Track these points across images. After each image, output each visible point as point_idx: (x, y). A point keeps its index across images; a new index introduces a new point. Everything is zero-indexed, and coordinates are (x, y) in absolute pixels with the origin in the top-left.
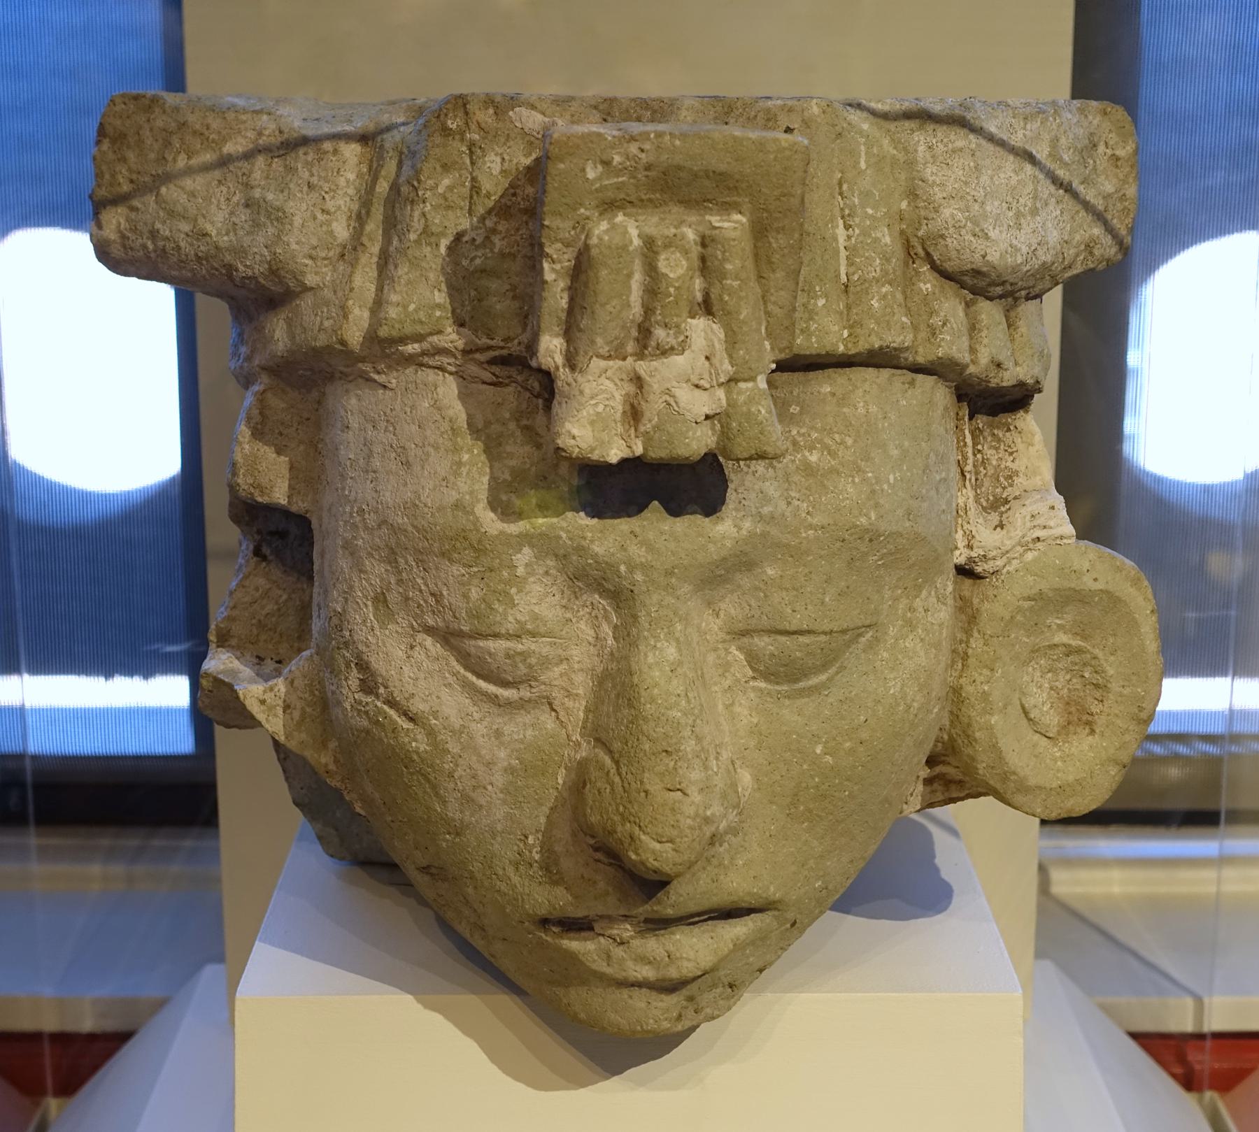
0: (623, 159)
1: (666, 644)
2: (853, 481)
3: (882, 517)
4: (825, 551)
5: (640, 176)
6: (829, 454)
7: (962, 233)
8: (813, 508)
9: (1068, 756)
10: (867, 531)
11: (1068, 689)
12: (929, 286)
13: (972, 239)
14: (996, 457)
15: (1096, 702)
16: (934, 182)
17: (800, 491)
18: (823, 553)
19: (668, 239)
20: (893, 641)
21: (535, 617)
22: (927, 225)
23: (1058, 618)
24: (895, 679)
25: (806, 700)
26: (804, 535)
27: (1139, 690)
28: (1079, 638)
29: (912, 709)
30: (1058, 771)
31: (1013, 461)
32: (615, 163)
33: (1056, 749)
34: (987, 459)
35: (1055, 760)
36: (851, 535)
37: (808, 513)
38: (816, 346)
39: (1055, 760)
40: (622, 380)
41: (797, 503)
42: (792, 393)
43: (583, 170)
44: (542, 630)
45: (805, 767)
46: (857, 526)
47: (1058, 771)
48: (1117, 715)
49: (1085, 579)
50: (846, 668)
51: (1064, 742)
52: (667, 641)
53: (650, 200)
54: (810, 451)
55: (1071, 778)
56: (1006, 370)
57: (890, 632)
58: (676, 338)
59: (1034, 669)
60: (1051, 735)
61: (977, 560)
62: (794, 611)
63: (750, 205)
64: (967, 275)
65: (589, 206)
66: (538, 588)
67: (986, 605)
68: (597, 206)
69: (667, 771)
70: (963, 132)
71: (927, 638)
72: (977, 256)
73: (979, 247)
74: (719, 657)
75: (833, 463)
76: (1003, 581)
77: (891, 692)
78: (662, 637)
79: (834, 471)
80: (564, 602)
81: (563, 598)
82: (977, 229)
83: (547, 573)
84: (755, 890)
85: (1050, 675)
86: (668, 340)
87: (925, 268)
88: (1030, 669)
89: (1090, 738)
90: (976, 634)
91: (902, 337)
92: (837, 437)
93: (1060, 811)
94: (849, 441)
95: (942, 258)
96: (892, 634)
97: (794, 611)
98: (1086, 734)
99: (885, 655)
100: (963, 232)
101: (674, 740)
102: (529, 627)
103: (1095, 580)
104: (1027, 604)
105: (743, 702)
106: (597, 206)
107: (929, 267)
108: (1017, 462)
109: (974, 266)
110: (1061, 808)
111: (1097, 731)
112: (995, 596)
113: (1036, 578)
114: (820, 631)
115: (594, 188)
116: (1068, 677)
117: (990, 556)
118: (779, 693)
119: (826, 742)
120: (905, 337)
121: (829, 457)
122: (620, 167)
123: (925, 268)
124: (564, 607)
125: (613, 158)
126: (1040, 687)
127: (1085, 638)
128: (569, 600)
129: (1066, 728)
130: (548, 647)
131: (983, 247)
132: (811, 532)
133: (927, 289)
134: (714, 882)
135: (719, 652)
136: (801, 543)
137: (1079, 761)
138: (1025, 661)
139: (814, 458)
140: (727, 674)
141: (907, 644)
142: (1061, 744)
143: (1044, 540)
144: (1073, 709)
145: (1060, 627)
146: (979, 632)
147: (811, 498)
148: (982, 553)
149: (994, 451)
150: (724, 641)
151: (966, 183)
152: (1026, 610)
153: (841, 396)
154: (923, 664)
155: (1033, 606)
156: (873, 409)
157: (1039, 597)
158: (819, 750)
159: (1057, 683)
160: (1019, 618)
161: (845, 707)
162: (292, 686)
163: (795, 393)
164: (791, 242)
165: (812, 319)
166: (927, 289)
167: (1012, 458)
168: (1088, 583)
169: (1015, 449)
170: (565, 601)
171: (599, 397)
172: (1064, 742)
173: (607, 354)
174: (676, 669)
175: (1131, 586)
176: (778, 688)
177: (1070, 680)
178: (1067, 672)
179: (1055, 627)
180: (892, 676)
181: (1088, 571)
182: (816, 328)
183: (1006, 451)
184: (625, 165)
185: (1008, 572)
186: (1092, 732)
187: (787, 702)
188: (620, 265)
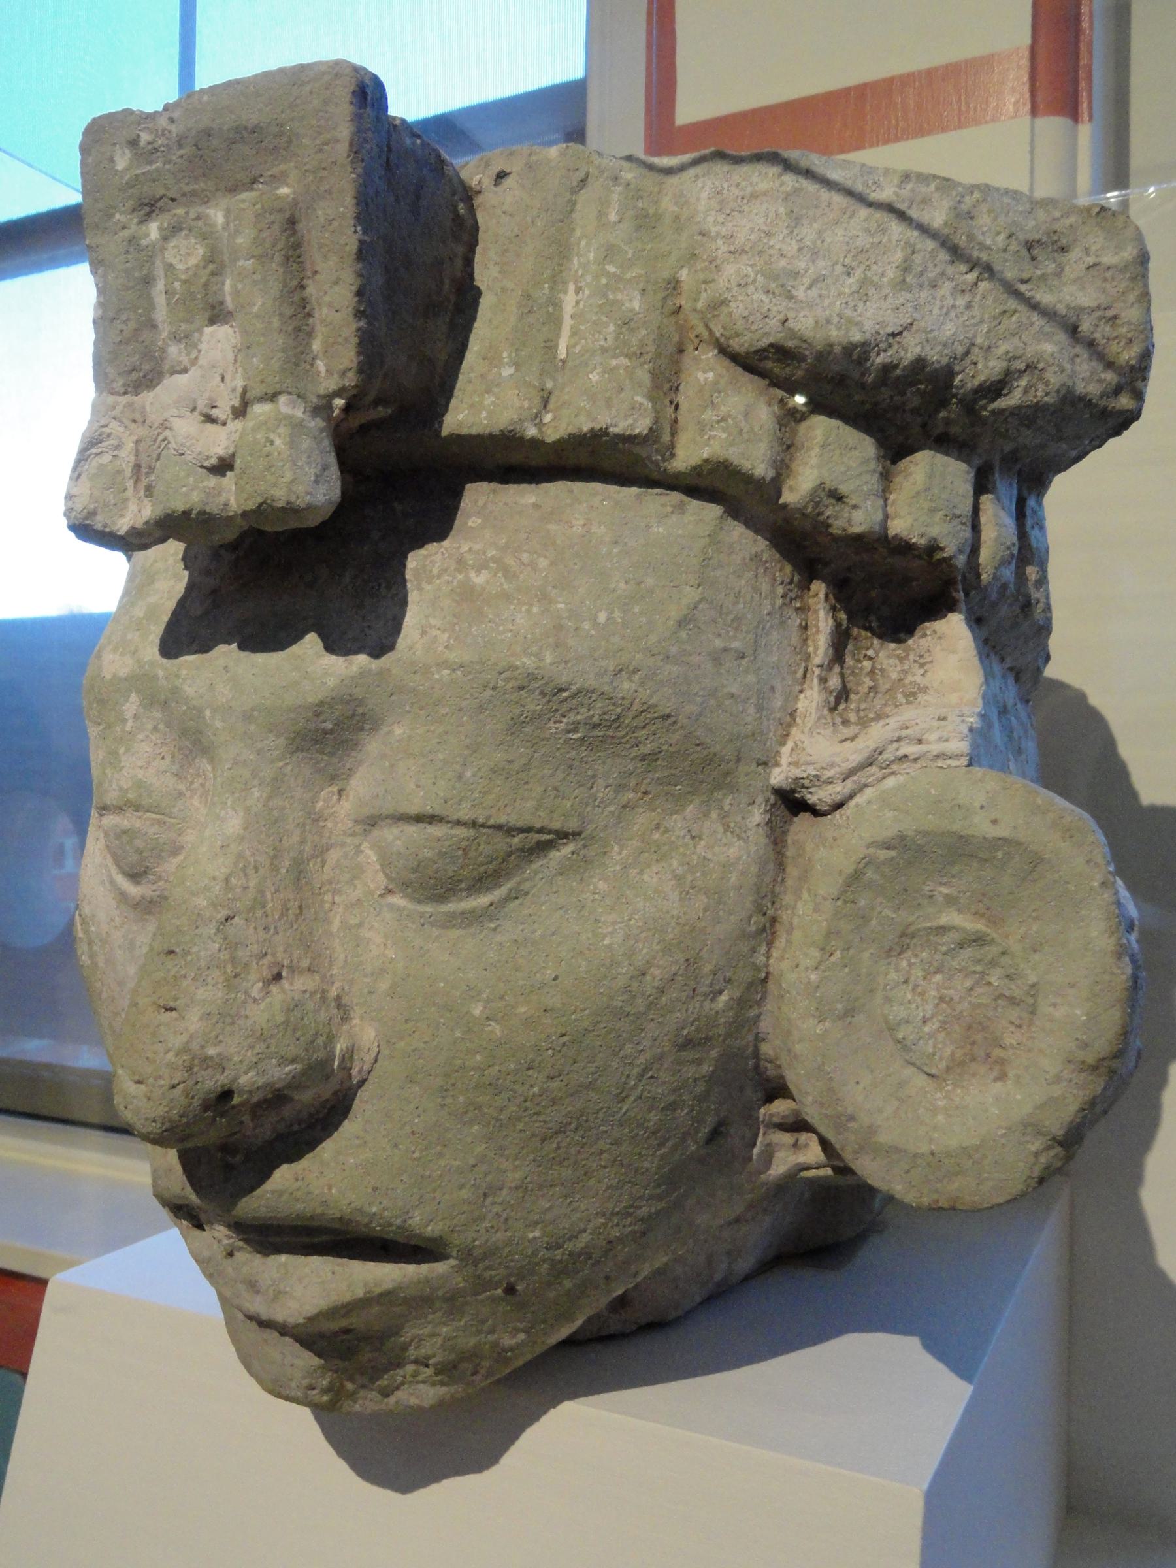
0: (153, 136)
1: (231, 812)
2: (528, 611)
3: (566, 662)
4: (468, 702)
5: (174, 158)
6: (505, 576)
7: (749, 292)
8: (455, 639)
9: (957, 1108)
10: (532, 677)
11: (970, 1002)
12: (711, 375)
13: (764, 297)
14: (899, 668)
15: (1012, 1028)
16: (718, 234)
17: (445, 618)
18: (464, 703)
19: (176, 218)
20: (618, 868)
21: (139, 784)
22: (706, 290)
23: (941, 884)
24: (614, 923)
25: (461, 932)
26: (437, 676)
27: (1078, 1012)
28: (983, 921)
29: (648, 978)
30: (935, 1128)
31: (923, 675)
32: (142, 143)
33: (939, 1095)
34: (882, 670)
35: (934, 1111)
36: (507, 680)
37: (446, 647)
38: (486, 422)
39: (934, 1111)
40: (134, 421)
41: (434, 632)
42: (476, 502)
43: (112, 160)
44: (146, 802)
45: (458, 1034)
46: (517, 668)
47: (935, 1128)
48: (1041, 1051)
49: (977, 819)
50: (527, 893)
51: (955, 1085)
52: (233, 809)
53: (193, 193)
54: (478, 572)
55: (953, 1143)
56: (855, 507)
57: (614, 854)
58: (188, 354)
59: (910, 965)
60: (933, 1071)
61: (806, 783)
62: (418, 786)
63: (297, 171)
64: (767, 358)
65: (123, 209)
66: (146, 747)
67: (822, 852)
68: (134, 210)
69: (165, 979)
70: (773, 170)
71: (689, 878)
72: (774, 323)
73: (775, 309)
74: (345, 855)
75: (505, 587)
76: (848, 817)
77: (606, 942)
78: (229, 803)
79: (506, 597)
80: (175, 768)
81: (173, 762)
82: (773, 285)
83: (155, 728)
84: (374, 1210)
85: (938, 978)
86: (181, 359)
87: (710, 355)
88: (904, 963)
89: (999, 1084)
90: (805, 895)
91: (630, 421)
92: (525, 557)
93: (935, 1196)
94: (543, 563)
95: (727, 334)
96: (618, 858)
97: (418, 786)
98: (992, 1077)
99: (602, 885)
100: (751, 289)
101: (188, 938)
102: (131, 796)
103: (994, 822)
104: (883, 854)
105: (376, 924)
106: (134, 210)
107: (716, 352)
108: (929, 675)
109: (771, 340)
110: (937, 1191)
111: (1011, 1075)
112: (835, 840)
113: (896, 813)
114: (455, 818)
115: (124, 182)
116: (968, 983)
117: (825, 777)
118: (422, 915)
119: (488, 1001)
120: (636, 421)
121: (503, 580)
122: (150, 147)
123: (710, 355)
124: (176, 775)
125: (138, 136)
126: (922, 994)
127: (994, 922)
128: (182, 767)
129: (958, 1067)
130: (157, 826)
131: (781, 308)
132: (446, 672)
133: (706, 379)
134: (297, 1180)
135: (347, 849)
136: (433, 688)
137: (974, 1118)
138: (891, 949)
139: (479, 579)
140: (356, 882)
141: (646, 877)
142: (949, 1088)
143: (916, 760)
144: (979, 1037)
145: (950, 901)
146: (809, 890)
147: (457, 628)
148: (814, 773)
149: (897, 661)
150: (354, 834)
151: (768, 234)
152: (883, 863)
153: (550, 509)
154: (675, 912)
155: (893, 859)
156: (599, 530)
157: (900, 843)
158: (477, 1010)
159: (951, 992)
160: (870, 874)
161: (523, 952)
162: (78, 905)
163: (480, 503)
164: (341, 209)
165: (488, 391)
166: (706, 379)
167: (922, 671)
168: (981, 826)
169: (929, 659)
170: (177, 766)
171: (104, 444)
172: (955, 1085)
173: (123, 390)
174: (228, 846)
175: (1063, 839)
176: (421, 908)
177: (971, 989)
178: (966, 976)
179: (941, 899)
180: (610, 918)
181: (982, 807)
182: (492, 402)
183: (915, 661)
184: (156, 145)
185: (857, 805)
186: (1002, 1077)
187: (435, 932)
188: (128, 265)
